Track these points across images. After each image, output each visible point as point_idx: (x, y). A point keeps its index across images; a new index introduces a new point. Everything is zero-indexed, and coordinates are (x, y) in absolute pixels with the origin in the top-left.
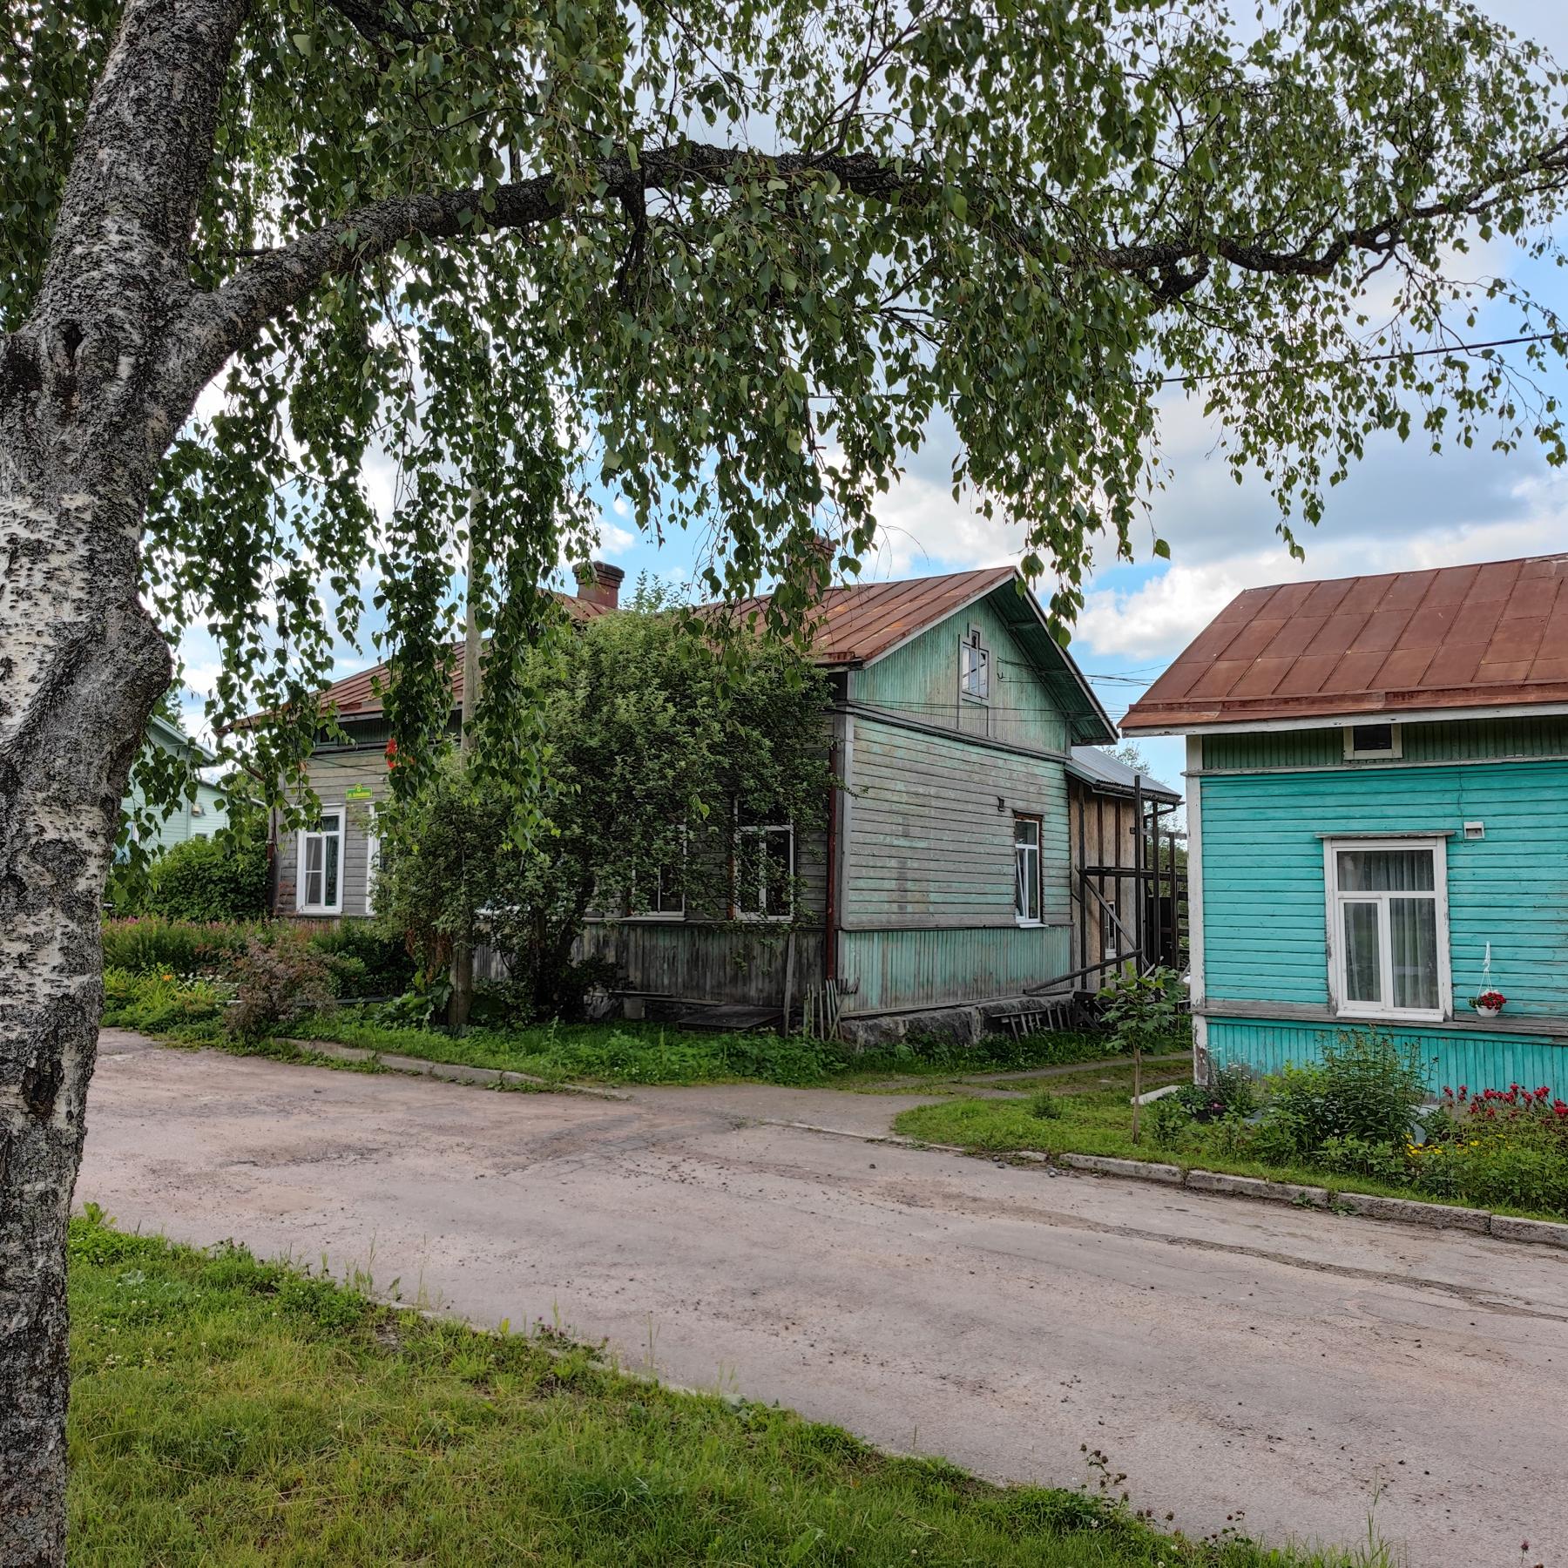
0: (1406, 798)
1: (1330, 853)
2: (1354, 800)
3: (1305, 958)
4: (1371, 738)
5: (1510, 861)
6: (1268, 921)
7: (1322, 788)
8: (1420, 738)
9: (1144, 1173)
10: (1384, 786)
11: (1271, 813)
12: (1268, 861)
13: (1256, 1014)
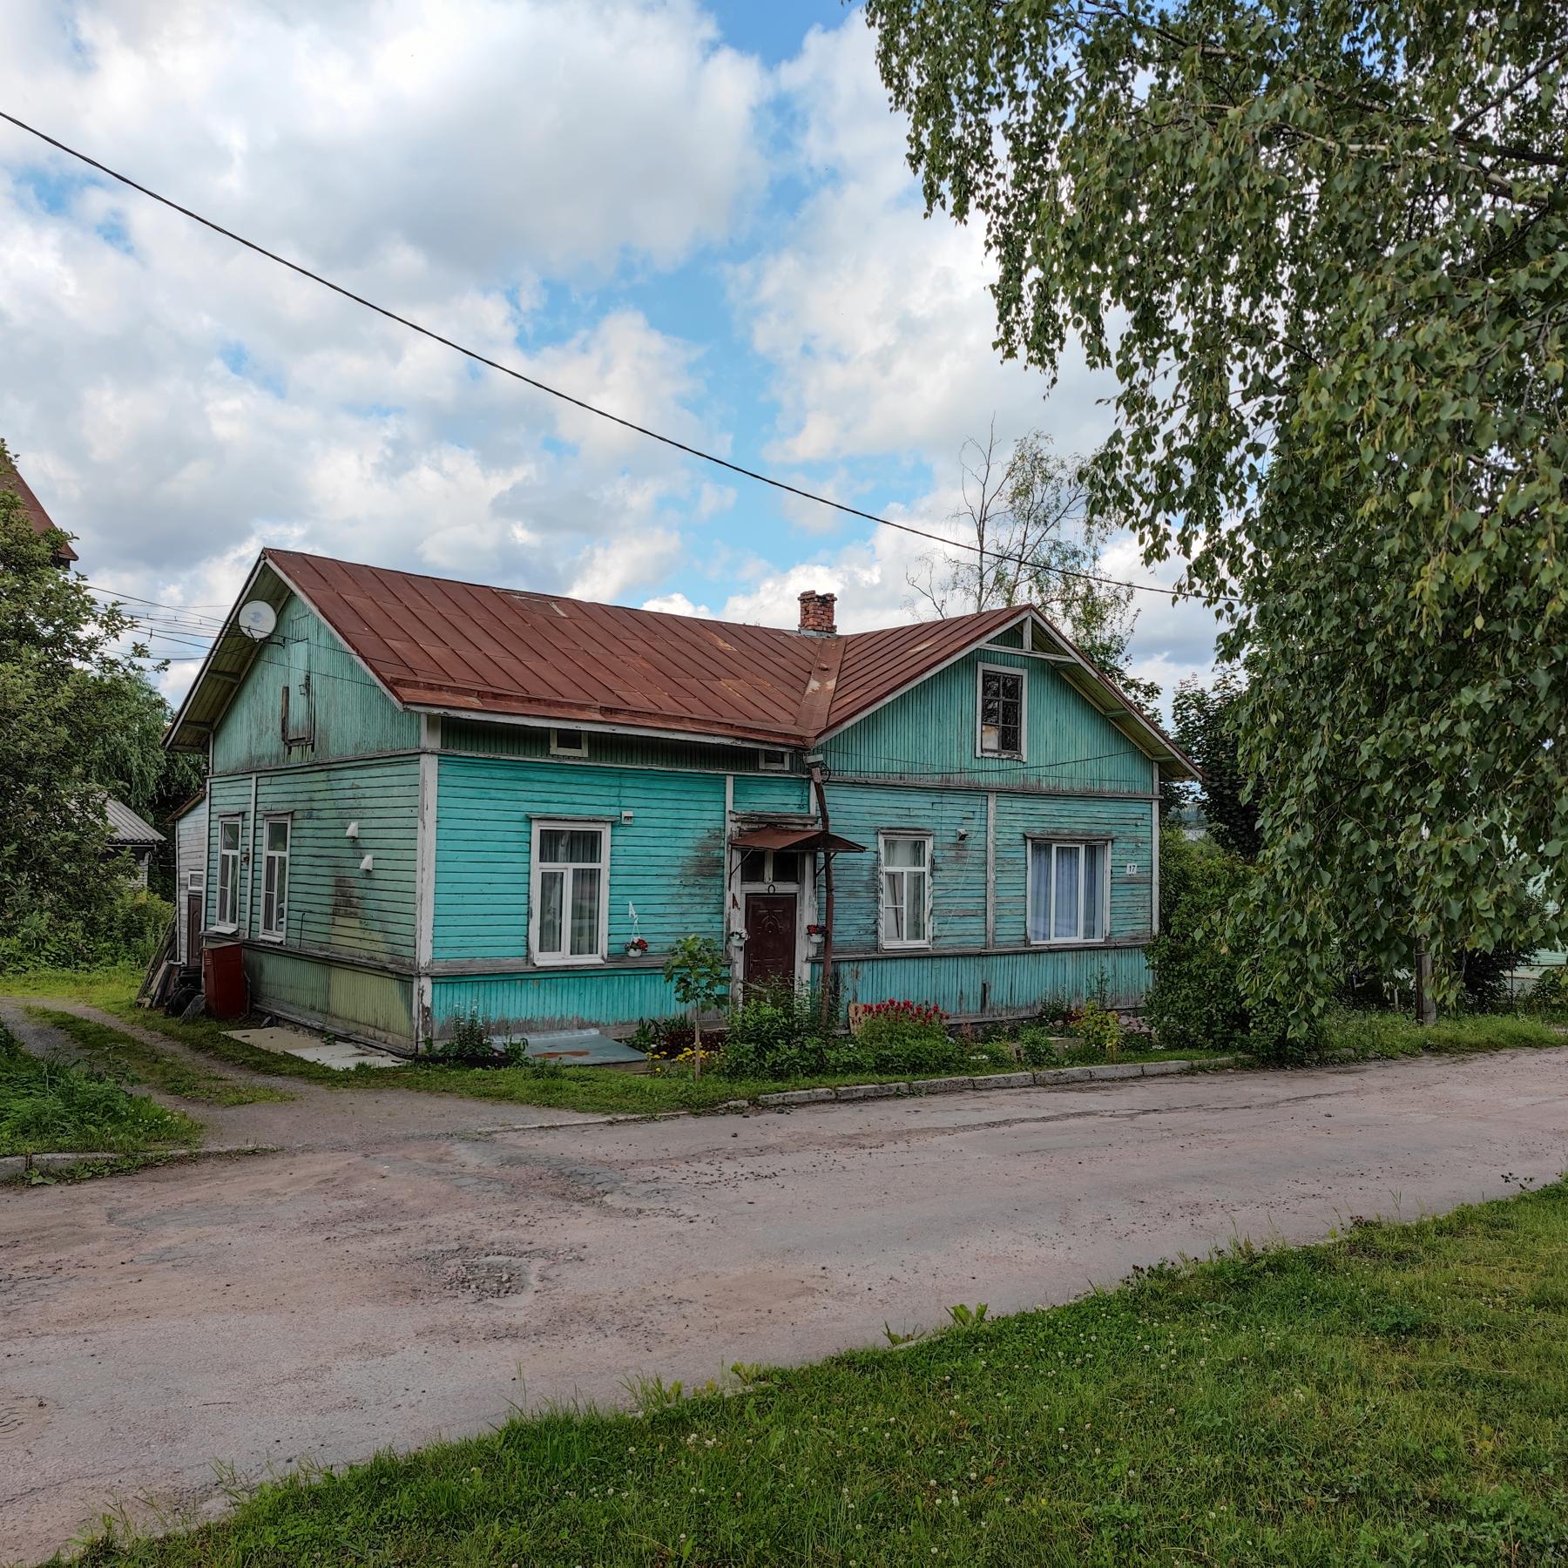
0: (587, 789)
1: (536, 829)
2: (554, 787)
3: (512, 919)
4: (569, 739)
5: (646, 842)
6: (487, 888)
7: (531, 775)
8: (603, 745)
9: (814, 1097)
10: (573, 778)
11: (494, 794)
12: (490, 835)
13: (476, 970)
